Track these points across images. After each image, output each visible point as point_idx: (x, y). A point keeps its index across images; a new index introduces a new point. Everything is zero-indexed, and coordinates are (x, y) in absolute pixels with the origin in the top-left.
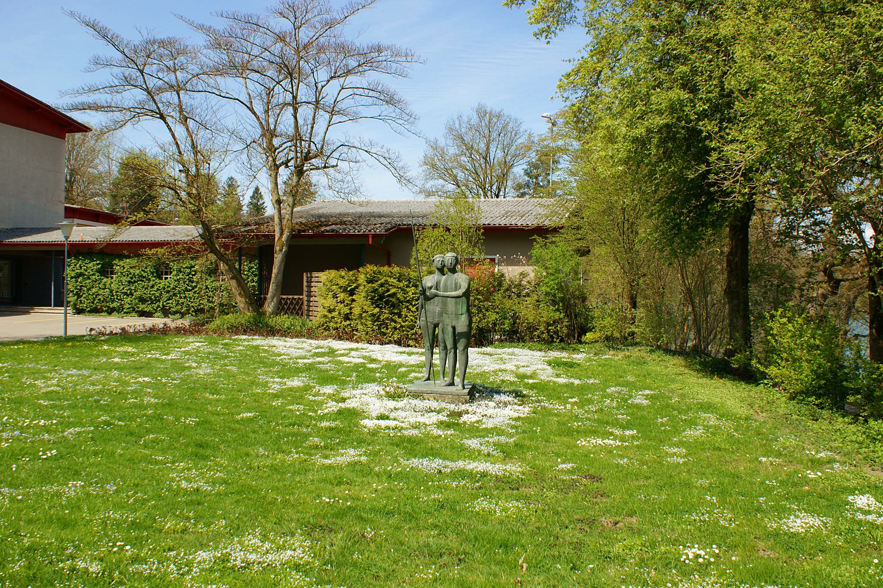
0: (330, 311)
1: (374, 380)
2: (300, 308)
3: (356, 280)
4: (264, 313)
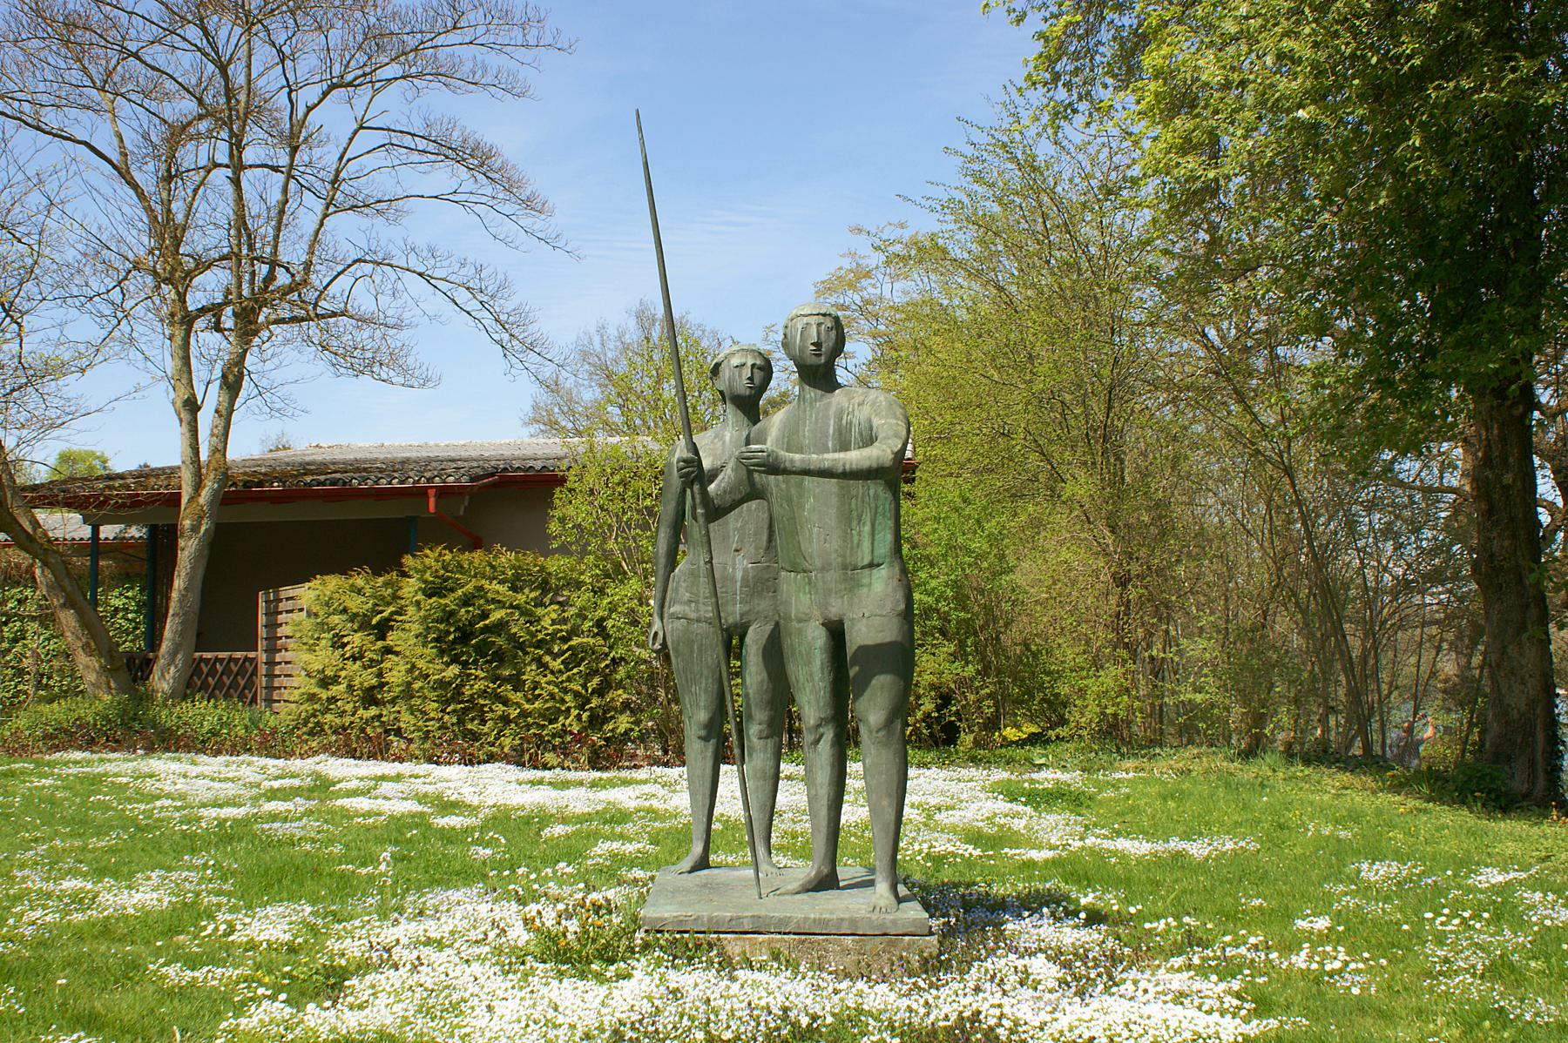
0: (325, 683)
1: (467, 874)
2: (250, 684)
3: (395, 597)
4: (150, 697)
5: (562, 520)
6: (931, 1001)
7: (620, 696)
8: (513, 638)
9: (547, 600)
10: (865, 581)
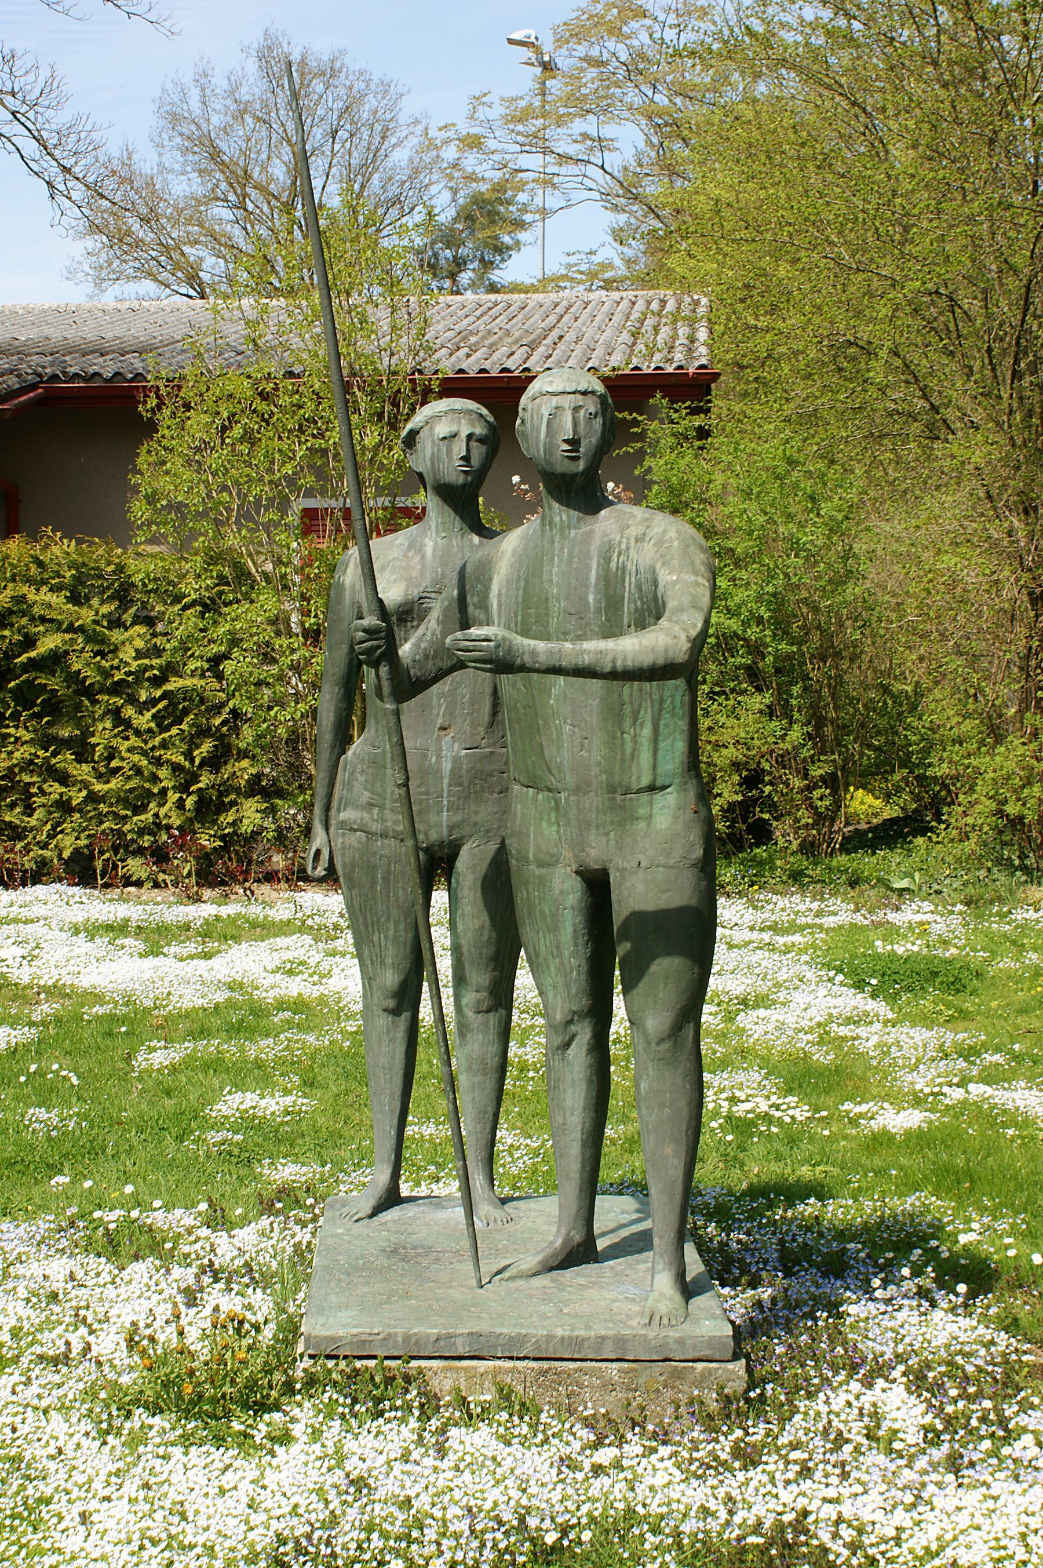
5: (151, 499)
6: (735, 1493)
7: (244, 770)
8: (74, 678)
9: (127, 618)
10: (642, 811)
